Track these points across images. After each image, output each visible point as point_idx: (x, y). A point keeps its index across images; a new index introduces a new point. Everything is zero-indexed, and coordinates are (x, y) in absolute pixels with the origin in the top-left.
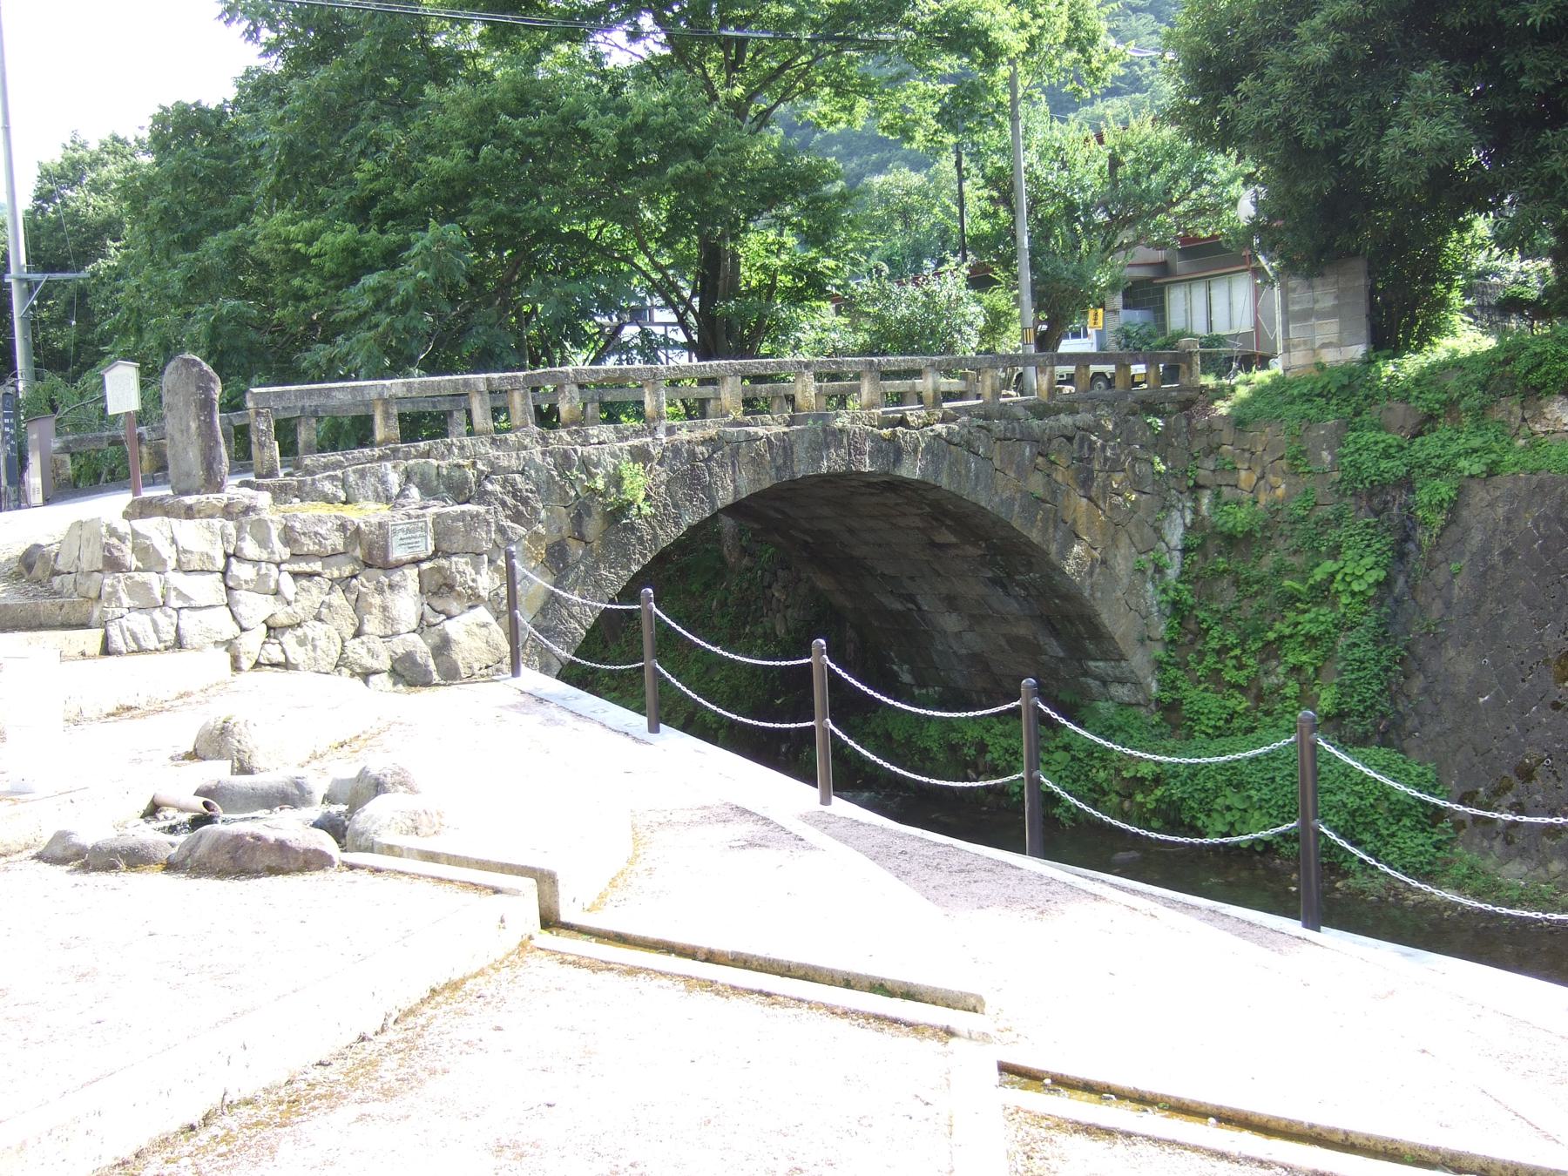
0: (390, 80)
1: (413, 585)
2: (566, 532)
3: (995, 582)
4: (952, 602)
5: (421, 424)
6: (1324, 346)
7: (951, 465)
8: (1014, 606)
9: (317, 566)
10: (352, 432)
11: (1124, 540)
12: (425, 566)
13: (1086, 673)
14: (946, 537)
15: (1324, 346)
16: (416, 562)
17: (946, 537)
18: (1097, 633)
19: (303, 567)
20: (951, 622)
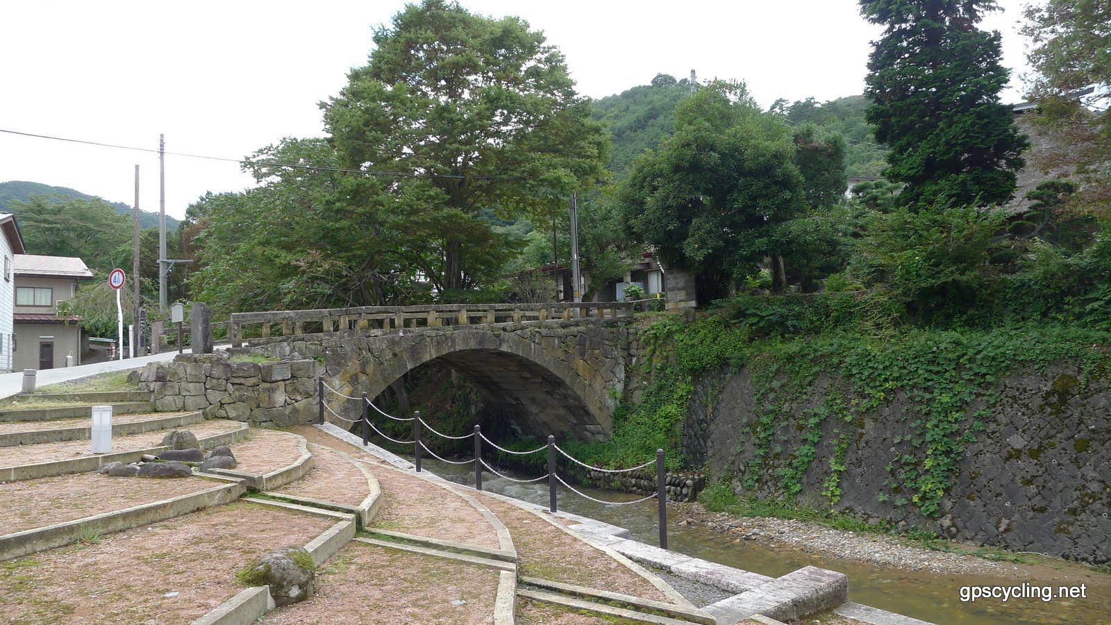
0: (406, 150)
1: (282, 388)
2: (358, 370)
3: (547, 392)
4: (533, 400)
5: (314, 327)
6: (680, 301)
7: (524, 347)
8: (556, 403)
9: (242, 381)
10: (276, 331)
11: (599, 377)
12: (287, 382)
13: (586, 430)
14: (527, 375)
15: (680, 301)
16: (284, 380)
17: (527, 375)
18: (587, 413)
19: (237, 381)
20: (533, 409)
